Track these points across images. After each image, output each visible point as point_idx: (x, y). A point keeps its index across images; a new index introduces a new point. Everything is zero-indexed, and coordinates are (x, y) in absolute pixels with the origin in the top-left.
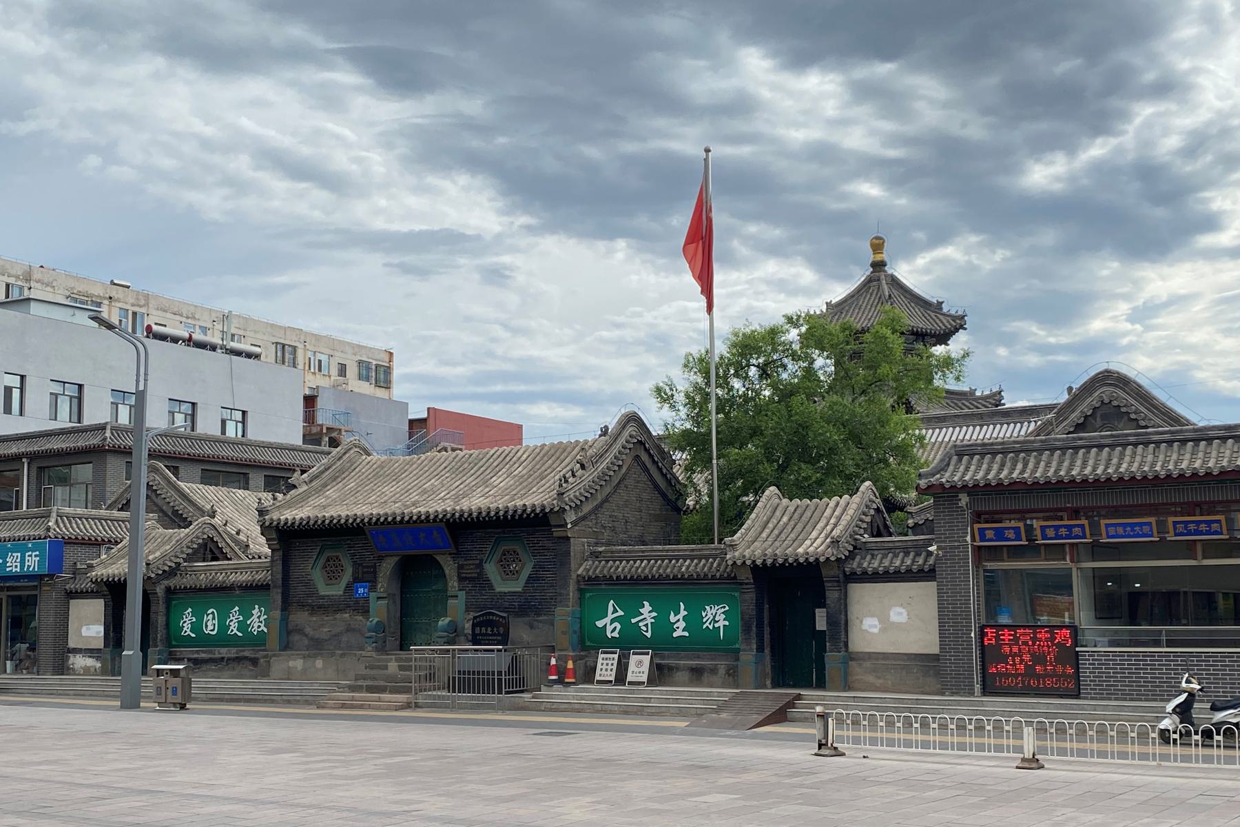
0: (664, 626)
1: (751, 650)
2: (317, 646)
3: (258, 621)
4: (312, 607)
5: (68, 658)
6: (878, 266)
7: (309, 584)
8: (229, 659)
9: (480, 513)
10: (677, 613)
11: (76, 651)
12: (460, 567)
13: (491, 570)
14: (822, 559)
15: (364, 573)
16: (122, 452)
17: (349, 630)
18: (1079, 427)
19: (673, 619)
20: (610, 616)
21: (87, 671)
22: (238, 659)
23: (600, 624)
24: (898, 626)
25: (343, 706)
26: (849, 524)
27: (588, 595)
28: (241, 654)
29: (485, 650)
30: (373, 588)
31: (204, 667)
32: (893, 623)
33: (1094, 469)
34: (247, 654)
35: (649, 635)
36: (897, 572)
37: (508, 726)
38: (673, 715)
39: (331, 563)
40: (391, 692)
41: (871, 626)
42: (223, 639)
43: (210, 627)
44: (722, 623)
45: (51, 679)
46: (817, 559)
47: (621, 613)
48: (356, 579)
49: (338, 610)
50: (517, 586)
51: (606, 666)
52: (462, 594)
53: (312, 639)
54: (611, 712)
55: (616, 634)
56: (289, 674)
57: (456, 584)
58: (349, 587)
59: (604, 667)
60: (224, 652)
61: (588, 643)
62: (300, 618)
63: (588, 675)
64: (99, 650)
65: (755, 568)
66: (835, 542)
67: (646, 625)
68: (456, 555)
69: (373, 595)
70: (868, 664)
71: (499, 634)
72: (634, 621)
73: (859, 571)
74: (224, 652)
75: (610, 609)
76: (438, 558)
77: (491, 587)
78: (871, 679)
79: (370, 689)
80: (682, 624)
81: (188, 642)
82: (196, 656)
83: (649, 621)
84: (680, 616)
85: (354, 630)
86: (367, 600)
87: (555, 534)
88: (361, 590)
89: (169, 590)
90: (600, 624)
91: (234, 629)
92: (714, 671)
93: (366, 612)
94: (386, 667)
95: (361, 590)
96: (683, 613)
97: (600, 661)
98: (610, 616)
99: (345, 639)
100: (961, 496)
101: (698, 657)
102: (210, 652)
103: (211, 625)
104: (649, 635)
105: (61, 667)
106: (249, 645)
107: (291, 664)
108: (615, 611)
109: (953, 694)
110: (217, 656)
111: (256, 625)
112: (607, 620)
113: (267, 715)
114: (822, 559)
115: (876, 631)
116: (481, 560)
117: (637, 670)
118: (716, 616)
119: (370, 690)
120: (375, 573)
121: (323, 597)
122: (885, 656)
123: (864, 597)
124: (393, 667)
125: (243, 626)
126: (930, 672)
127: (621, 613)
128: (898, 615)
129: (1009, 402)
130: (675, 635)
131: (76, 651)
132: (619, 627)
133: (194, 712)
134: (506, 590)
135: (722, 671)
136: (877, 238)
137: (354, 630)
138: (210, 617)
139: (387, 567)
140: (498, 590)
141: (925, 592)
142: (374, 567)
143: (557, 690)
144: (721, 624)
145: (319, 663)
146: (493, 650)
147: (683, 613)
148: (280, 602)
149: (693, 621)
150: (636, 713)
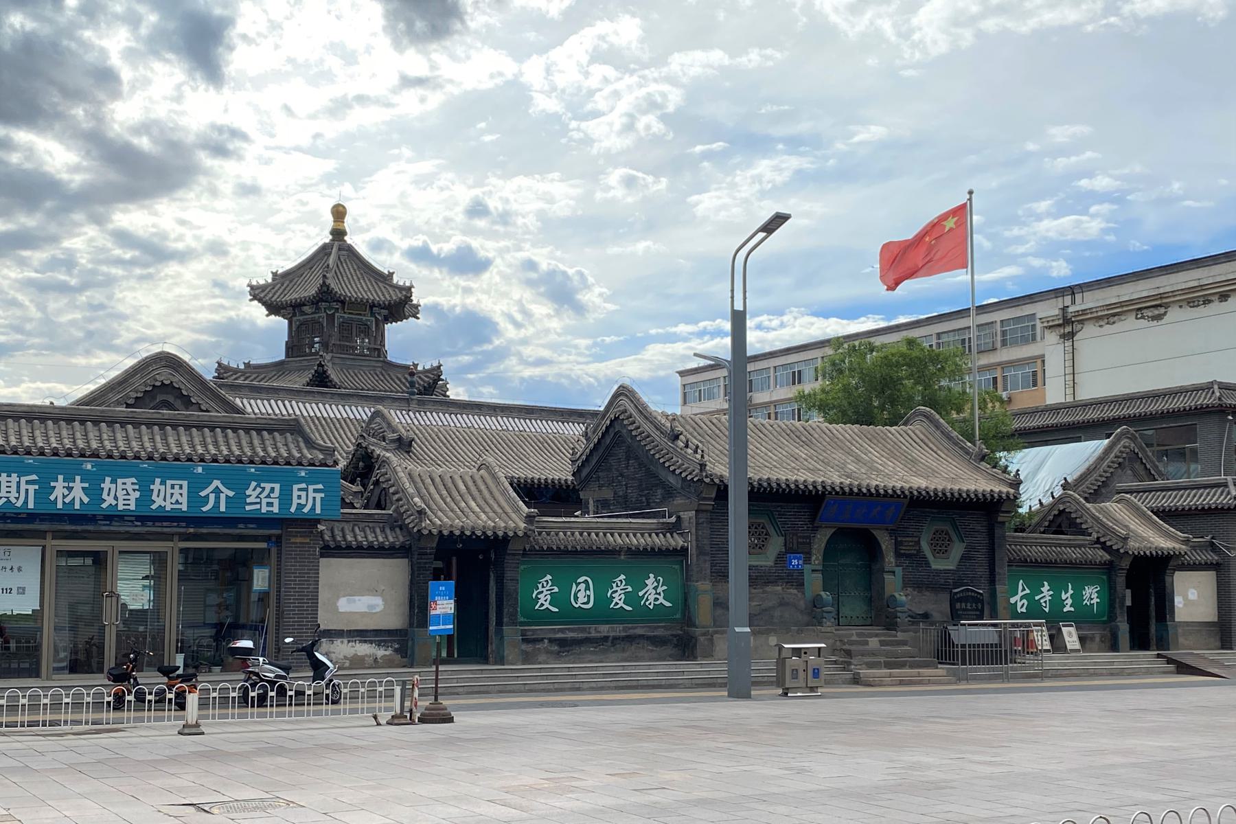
0: (1057, 602)
3: (654, 592)
6: (338, 234)
8: (615, 638)
11: (332, 634)
12: (897, 544)
16: (1150, 419)
17: (783, 604)
18: (138, 402)
19: (1064, 597)
20: (1020, 594)
21: (357, 662)
22: (630, 639)
23: (1012, 600)
25: (901, 683)
28: (631, 632)
30: (807, 560)
31: (577, 650)
34: (639, 631)
35: (1047, 610)
40: (911, 667)
42: (602, 612)
43: (582, 599)
46: (462, 533)
47: (1028, 591)
48: (789, 550)
49: (768, 583)
50: (951, 566)
52: (899, 570)
54: (1101, 675)
55: (1024, 610)
57: (892, 560)
58: (780, 558)
60: (604, 629)
68: (892, 532)
71: (977, 610)
74: (604, 629)
77: (928, 564)
79: (888, 665)
80: (1069, 601)
83: (1048, 598)
85: (787, 604)
86: (801, 573)
88: (795, 562)
90: (1012, 600)
91: (619, 600)
93: (801, 585)
94: (867, 643)
95: (795, 562)
96: (1071, 592)
98: (1020, 594)
99: (777, 613)
102: (584, 630)
103: (583, 595)
104: (1047, 610)
106: (642, 621)
108: (1024, 589)
110: (594, 634)
111: (651, 598)
112: (1017, 597)
113: (996, 691)
123: (333, 571)
124: (874, 643)
125: (630, 598)
126: (1222, 632)
127: (1028, 591)
129: (456, 392)
131: (332, 634)
133: (759, 698)
135: (1098, 639)
136: (339, 205)
137: (787, 604)
138: (582, 586)
139: (821, 539)
140: (934, 567)
142: (809, 537)
144: (1095, 601)
147: (1071, 592)
149: (1077, 598)
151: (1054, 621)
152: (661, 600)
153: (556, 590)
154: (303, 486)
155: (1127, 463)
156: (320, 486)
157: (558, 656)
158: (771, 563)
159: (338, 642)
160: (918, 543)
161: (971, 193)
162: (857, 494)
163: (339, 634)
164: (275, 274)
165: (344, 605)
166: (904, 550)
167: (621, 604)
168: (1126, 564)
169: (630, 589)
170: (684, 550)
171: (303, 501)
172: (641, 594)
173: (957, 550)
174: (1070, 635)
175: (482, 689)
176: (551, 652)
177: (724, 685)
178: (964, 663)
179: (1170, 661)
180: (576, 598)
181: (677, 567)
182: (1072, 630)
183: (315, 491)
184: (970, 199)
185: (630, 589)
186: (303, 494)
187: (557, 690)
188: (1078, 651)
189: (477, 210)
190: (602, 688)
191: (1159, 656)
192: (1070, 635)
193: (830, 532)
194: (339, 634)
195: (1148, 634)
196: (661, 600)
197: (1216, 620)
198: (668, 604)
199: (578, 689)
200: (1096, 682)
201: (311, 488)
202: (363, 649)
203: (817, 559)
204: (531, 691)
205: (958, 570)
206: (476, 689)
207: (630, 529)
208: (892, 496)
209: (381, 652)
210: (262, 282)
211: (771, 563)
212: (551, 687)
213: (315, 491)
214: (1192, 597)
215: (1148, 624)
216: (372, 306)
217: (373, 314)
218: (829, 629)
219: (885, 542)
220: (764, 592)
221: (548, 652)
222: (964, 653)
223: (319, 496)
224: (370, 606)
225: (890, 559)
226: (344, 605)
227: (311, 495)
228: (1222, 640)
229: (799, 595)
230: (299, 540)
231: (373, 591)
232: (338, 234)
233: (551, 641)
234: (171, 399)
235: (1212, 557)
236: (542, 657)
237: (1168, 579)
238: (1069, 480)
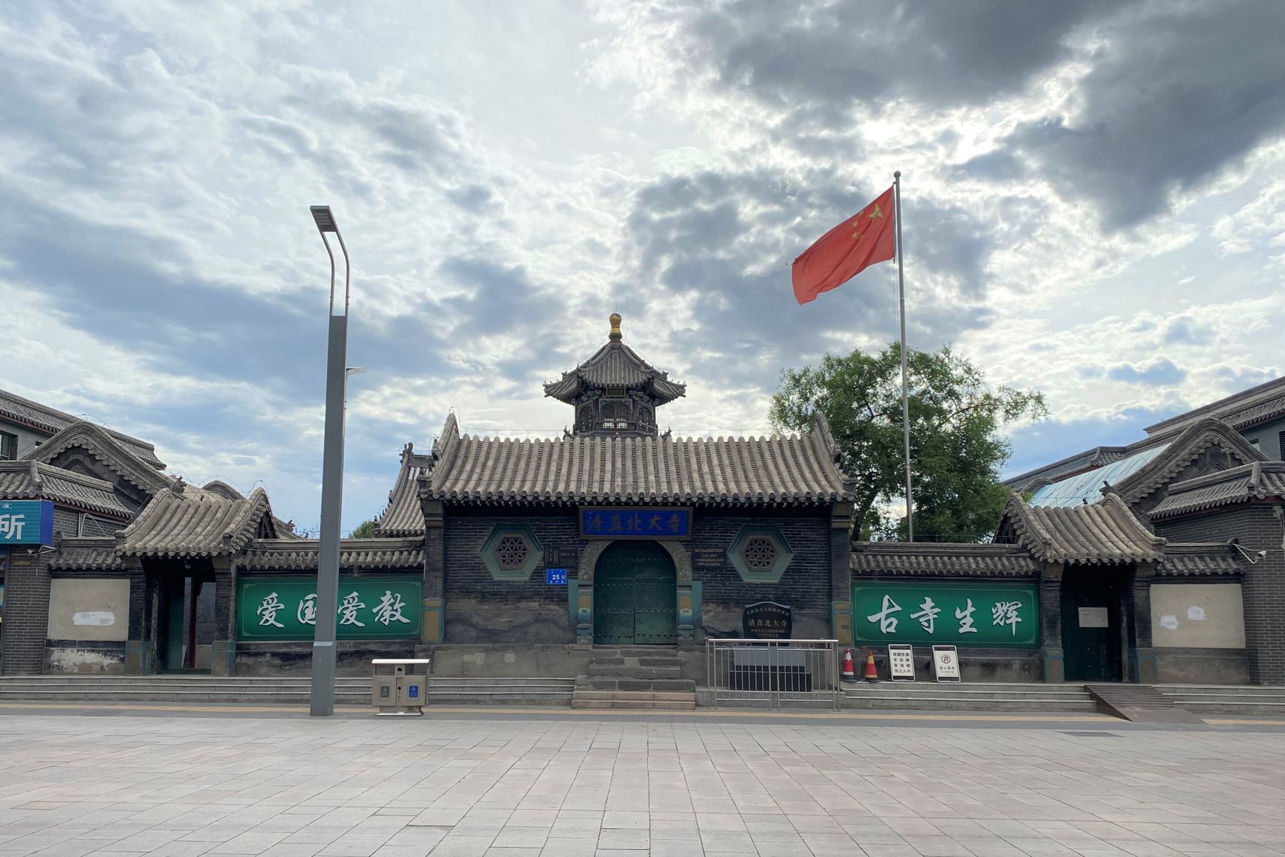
1: (1057, 645)
2: (491, 638)
4: (483, 595)
5: (48, 654)
6: (615, 337)
7: (478, 567)
9: (501, 497)
10: (964, 609)
11: (63, 644)
12: (695, 556)
13: (736, 559)
14: (214, 554)
15: (560, 557)
19: (958, 614)
20: (885, 611)
21: (85, 669)
23: (873, 619)
24: (1196, 624)
26: (1032, 528)
27: (246, 586)
28: (363, 647)
29: (754, 644)
30: (574, 572)
32: (1191, 621)
33: (534, 486)
35: (931, 630)
36: (99, 569)
37: (876, 725)
38: (1033, 710)
39: (508, 545)
41: (1169, 623)
44: (1014, 619)
45: (22, 680)
47: (898, 608)
48: (549, 565)
51: (902, 661)
52: (698, 586)
53: (483, 630)
54: (958, 709)
55: (892, 630)
56: (464, 671)
58: (538, 572)
59: (898, 662)
61: (245, 634)
62: (467, 606)
63: (883, 671)
64: (120, 644)
65: (145, 559)
66: (228, 538)
67: (928, 621)
68: (688, 544)
69: (572, 583)
70: (1169, 658)
72: (913, 616)
73: (74, 567)
75: (885, 603)
76: (664, 545)
78: (1173, 671)
80: (969, 621)
81: (271, 632)
82: (284, 650)
83: (931, 617)
84: (967, 613)
87: (834, 525)
88: (556, 577)
89: (242, 571)
90: (873, 619)
92: (1007, 666)
93: (563, 600)
96: (970, 609)
97: (892, 657)
98: (885, 611)
100: (1275, 508)
101: (989, 653)
104: (931, 630)
105: (42, 665)
107: (466, 658)
108: (891, 606)
109: (1271, 684)
111: (387, 615)
112: (882, 615)
114: (214, 554)
115: (1174, 627)
116: (725, 550)
117: (944, 665)
118: (1008, 613)
119: (632, 692)
120: (576, 557)
121: (500, 583)
122: (1185, 651)
125: (360, 615)
126: (1248, 663)
127: (898, 608)
128: (1196, 613)
130: (961, 631)
131: (63, 644)
132: (895, 622)
133: (339, 715)
134: (758, 581)
135: (1016, 666)
138: (310, 604)
140: (746, 580)
141: (1229, 595)
143: (861, 686)
145: (510, 658)
146: (765, 644)
147: (970, 609)
148: (440, 587)
149: (982, 617)
150: (989, 709)
151: (923, 645)
152: (398, 616)
153: (282, 606)
154: (7, 516)
155: (1208, 460)
156: (22, 516)
157: (983, 678)
158: (527, 579)
159: (68, 651)
160: (723, 555)
161: (897, 175)
162: (627, 504)
163: (72, 644)
164: (564, 375)
165: (78, 619)
166: (701, 562)
167: (272, 621)
168: (1056, 575)
169: (363, 606)
170: (420, 567)
171: (6, 530)
172: (375, 610)
173: (783, 561)
174: (946, 662)
175: (135, 696)
176: (274, 666)
177: (307, 701)
178: (774, 689)
179: (1093, 696)
180: (303, 615)
181: (418, 584)
182: (953, 655)
183: (17, 520)
184: (897, 183)
185: (363, 606)
186: (7, 523)
187: (211, 701)
188: (956, 679)
189: (1178, 334)
190: (261, 701)
191: (1086, 689)
192: (946, 662)
193: (602, 546)
194: (72, 644)
195: (1120, 662)
196: (398, 616)
197: (1243, 646)
198: (405, 620)
199: (235, 701)
200: (775, 715)
201: (14, 518)
202: (91, 658)
203: (586, 570)
204: (184, 700)
205: (782, 583)
206: (129, 696)
207: (371, 548)
208: (636, 504)
209: (107, 661)
210: (554, 382)
211: (527, 579)
212: (206, 697)
213: (17, 520)
214: (1189, 617)
215: (1120, 653)
216: (628, 389)
217: (630, 396)
218: (583, 647)
219: (680, 555)
220: (517, 608)
221: (269, 665)
222: (774, 676)
223: (20, 524)
224: (102, 621)
225: (684, 573)
226: (78, 619)
227: (14, 524)
228: (1251, 674)
229: (562, 611)
230: (21, 563)
231: (106, 608)
232: (615, 337)
233: (274, 655)
234: (81, 457)
235: (1234, 566)
236: (264, 670)
237: (1138, 595)
238: (1111, 484)
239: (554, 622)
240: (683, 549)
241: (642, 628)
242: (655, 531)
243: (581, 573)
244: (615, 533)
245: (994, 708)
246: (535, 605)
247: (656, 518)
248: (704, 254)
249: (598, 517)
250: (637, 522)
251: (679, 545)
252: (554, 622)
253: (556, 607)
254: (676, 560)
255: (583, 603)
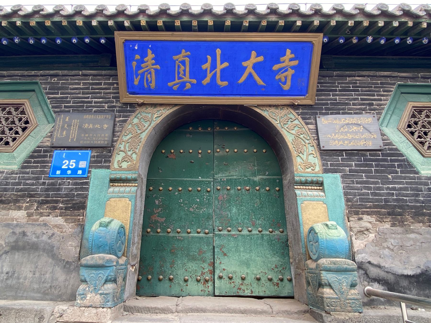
69: (99, 175)
76: (266, 113)
93: (75, 206)
158: (15, 167)
203: (131, 153)
211: (15, 167)
229: (69, 228)
239: (51, 252)
240: (299, 121)
241: (228, 265)
242: (250, 89)
243: (117, 158)
244: (181, 91)
245: (135, 213)
246: (19, 215)
247: (255, 58)
248: (251, 178)
249: (150, 55)
250: (220, 66)
251: (293, 114)
252: (51, 252)
253: (60, 220)
254: (289, 138)
255: (116, 210)
